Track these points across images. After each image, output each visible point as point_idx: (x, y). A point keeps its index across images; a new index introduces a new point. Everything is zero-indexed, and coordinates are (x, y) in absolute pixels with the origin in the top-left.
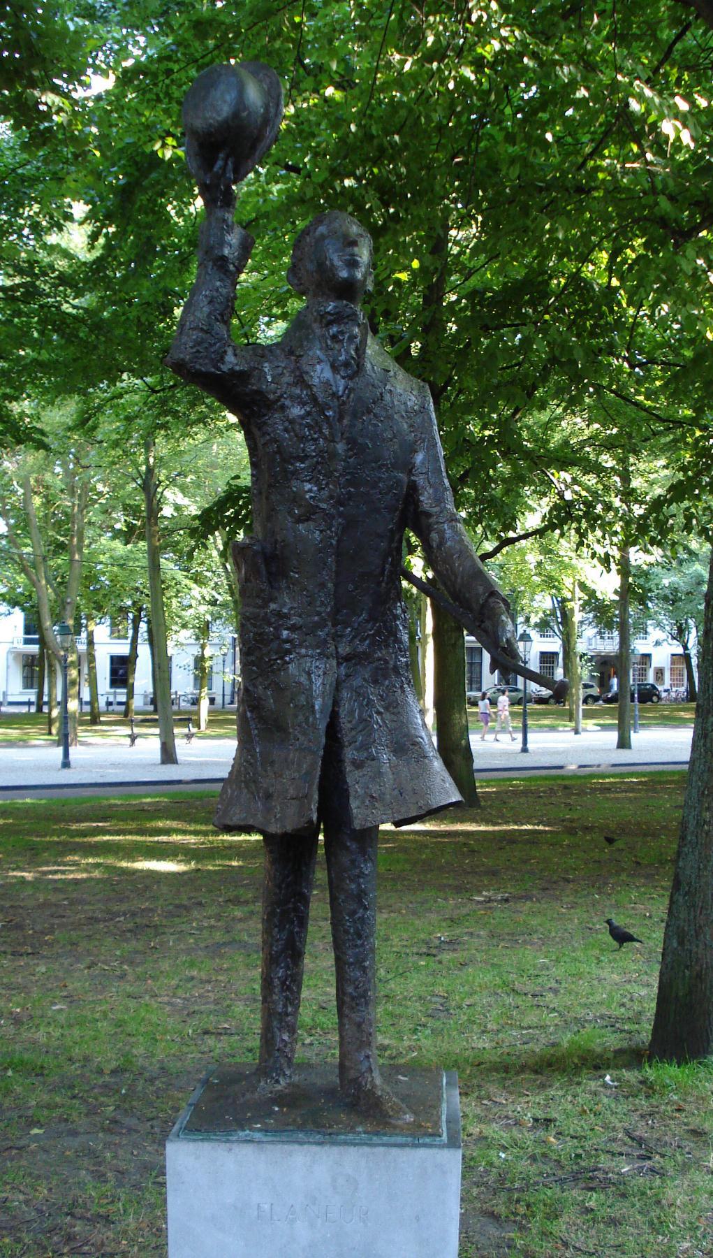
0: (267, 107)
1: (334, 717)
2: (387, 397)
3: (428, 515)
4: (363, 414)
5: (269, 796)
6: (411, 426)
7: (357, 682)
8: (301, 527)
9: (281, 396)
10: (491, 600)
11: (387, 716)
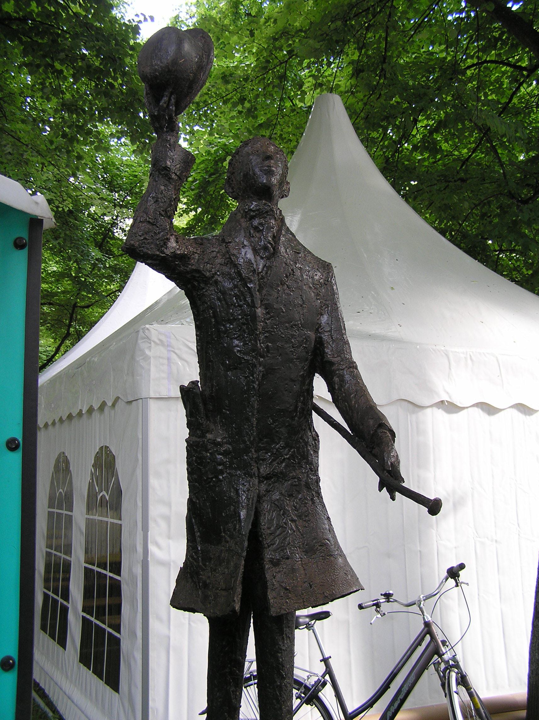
0: (201, 58)
1: (256, 524)
2: (298, 273)
3: (332, 364)
4: (278, 286)
5: (206, 586)
6: (318, 295)
7: (276, 496)
8: (229, 373)
9: (216, 273)
10: (380, 431)
11: (300, 523)
